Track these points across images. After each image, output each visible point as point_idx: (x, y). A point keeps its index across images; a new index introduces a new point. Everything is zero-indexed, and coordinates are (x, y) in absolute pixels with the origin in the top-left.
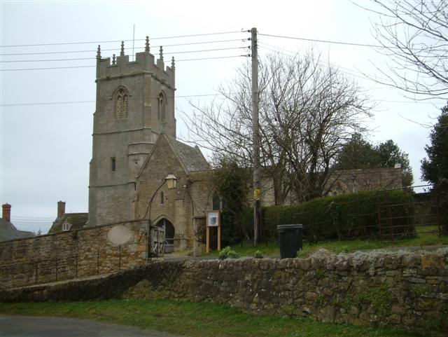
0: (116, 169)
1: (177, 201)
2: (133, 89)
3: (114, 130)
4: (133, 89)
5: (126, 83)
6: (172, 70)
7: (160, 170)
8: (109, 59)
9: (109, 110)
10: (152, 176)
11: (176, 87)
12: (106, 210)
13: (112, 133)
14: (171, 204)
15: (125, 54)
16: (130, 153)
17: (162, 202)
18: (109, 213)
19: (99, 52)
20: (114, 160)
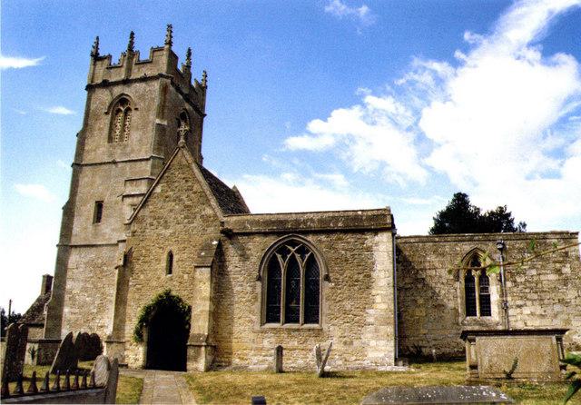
0: (103, 218)
1: (198, 270)
2: (434, 218)
3: (106, 159)
4: (434, 218)
5: (129, 91)
6: (203, 89)
7: (171, 211)
8: (317, 322)
9: (100, 129)
10: (155, 222)
11: (206, 112)
12: (82, 284)
13: (101, 164)
14: (186, 276)
15: (134, 50)
16: (127, 192)
17: (170, 272)
18: (85, 289)
19: (96, 48)
20: (99, 205)
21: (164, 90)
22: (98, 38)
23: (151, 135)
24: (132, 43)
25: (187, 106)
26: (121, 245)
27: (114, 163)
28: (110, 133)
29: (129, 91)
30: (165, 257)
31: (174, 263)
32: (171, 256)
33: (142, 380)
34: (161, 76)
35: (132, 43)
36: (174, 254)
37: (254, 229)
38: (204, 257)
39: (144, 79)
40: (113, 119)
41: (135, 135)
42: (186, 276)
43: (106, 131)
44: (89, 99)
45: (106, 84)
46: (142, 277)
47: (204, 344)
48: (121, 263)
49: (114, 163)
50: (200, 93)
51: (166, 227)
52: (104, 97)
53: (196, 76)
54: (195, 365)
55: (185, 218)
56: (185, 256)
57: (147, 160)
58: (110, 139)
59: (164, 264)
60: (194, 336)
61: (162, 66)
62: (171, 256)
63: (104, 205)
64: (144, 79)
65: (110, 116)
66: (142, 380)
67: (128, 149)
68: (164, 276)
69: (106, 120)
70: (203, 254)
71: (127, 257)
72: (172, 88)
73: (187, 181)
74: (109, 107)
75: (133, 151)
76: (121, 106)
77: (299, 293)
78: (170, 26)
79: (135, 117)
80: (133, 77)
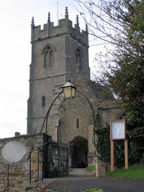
0: (46, 104)
1: (90, 125)
5: (52, 42)
7: (76, 101)
19: (33, 22)
21: (67, 40)
22: (33, 18)
23: (64, 63)
24: (49, 18)
25: (80, 45)
26: (55, 116)
27: (49, 77)
28: (45, 64)
29: (52, 42)
30: (75, 121)
31: (80, 124)
32: (78, 120)
33: (62, 147)
34: (65, 33)
35: (49, 18)
36: (79, 119)
37: (112, 107)
38: (91, 120)
39: (58, 35)
40: (45, 56)
41: (56, 64)
42: (85, 129)
43: (43, 63)
44: (66, 148)
45: (40, 40)
46: (67, 130)
47: (94, 156)
48: (58, 125)
49: (49, 77)
50: (85, 35)
51: (75, 108)
52: (41, 46)
53: (82, 27)
54: (91, 165)
55: (83, 104)
56: (84, 120)
57: (63, 75)
58: (45, 67)
59: (75, 124)
60: (90, 153)
61: (65, 30)
62: (78, 120)
63: (46, 98)
64: (58, 35)
65: (43, 55)
66: (62, 147)
67: (54, 71)
68: (76, 129)
69: (42, 57)
70: (91, 119)
71: (60, 122)
72: (71, 38)
73: (82, 88)
74: (43, 51)
75: (56, 71)
76: (48, 50)
77: (109, 149)
78: (67, 8)
79: (55, 54)
80: (52, 35)
